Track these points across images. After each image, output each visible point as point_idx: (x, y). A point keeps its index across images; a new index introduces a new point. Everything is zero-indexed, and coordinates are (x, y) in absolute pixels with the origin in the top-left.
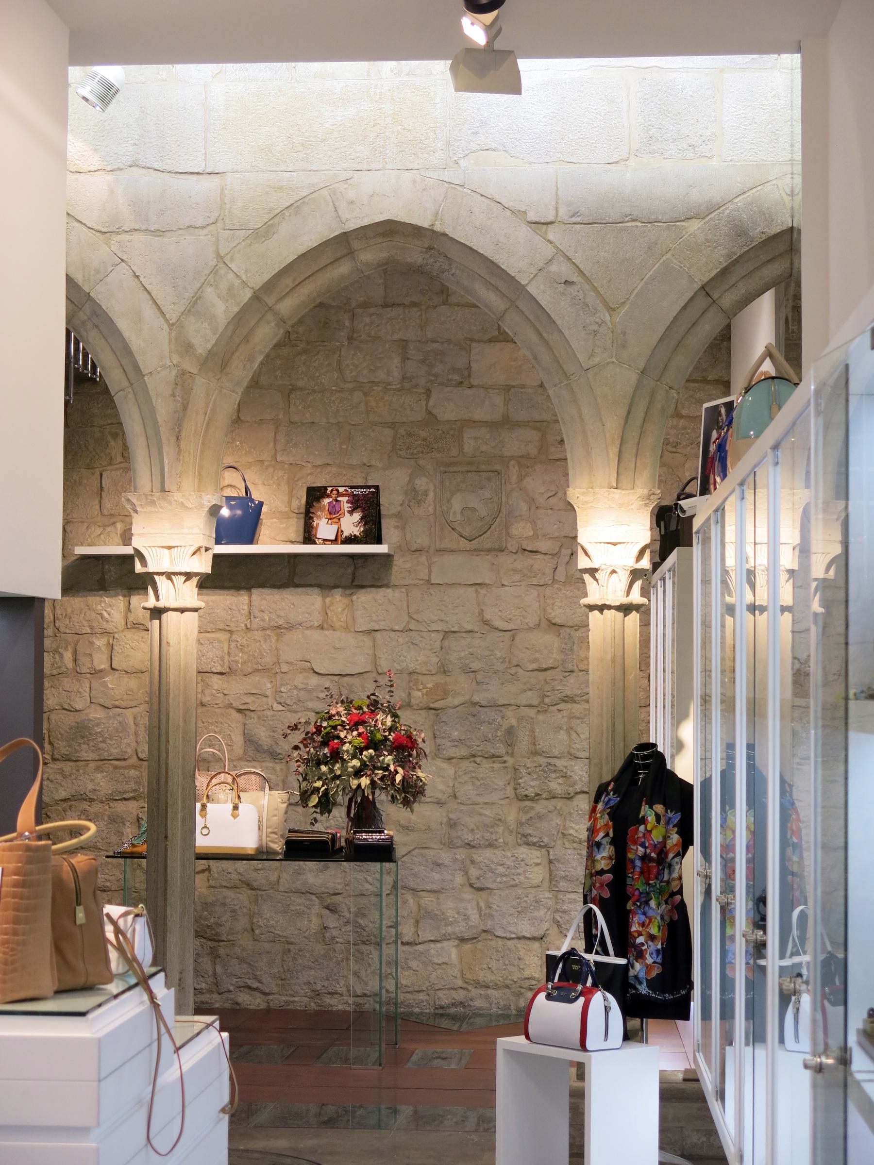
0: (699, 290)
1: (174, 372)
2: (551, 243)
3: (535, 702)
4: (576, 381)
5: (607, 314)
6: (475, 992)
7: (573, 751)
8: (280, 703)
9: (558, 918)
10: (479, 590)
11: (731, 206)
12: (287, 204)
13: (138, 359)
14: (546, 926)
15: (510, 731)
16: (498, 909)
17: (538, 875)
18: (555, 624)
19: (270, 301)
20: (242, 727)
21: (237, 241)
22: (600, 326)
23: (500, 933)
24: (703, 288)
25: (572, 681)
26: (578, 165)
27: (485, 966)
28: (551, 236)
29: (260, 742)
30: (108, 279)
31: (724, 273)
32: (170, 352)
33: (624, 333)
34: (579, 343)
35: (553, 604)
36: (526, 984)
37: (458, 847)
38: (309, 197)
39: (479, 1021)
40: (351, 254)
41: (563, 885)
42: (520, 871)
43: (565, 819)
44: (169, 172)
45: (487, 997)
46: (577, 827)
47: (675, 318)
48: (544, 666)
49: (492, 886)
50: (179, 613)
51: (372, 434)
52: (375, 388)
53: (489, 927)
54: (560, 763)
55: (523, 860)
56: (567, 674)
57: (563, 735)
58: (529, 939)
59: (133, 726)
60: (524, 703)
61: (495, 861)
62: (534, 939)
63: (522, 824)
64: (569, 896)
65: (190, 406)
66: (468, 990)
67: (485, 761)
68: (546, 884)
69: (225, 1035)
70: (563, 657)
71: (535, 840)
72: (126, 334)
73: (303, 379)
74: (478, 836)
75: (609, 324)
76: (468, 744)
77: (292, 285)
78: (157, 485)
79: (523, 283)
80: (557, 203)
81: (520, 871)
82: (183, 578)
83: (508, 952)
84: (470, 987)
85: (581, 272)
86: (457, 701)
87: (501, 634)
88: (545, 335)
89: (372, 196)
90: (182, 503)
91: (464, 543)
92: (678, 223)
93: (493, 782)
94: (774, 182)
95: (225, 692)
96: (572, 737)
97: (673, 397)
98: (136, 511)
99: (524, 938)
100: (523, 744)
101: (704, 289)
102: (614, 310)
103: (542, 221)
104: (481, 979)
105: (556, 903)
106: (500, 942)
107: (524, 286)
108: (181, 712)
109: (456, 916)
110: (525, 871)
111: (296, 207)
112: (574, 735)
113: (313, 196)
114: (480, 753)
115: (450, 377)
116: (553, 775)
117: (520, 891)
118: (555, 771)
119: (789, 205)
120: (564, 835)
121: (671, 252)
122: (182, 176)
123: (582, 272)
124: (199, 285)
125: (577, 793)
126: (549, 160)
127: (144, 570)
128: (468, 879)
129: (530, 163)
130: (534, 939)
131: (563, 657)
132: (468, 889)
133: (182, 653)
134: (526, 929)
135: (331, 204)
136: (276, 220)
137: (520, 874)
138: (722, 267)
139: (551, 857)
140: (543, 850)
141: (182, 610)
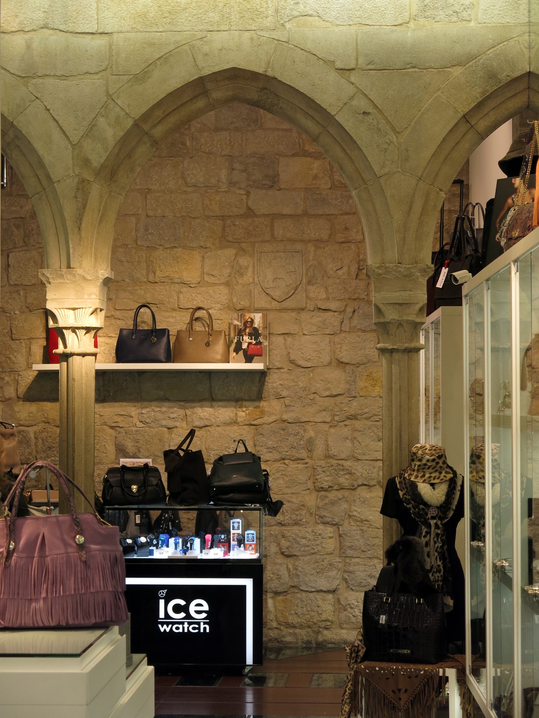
0: (462, 118)
1: (76, 180)
2: (353, 84)
3: (328, 419)
4: (372, 185)
5: (394, 137)
6: (285, 631)
7: (356, 455)
8: (142, 422)
9: (346, 577)
10: (286, 338)
11: (485, 57)
12: (158, 56)
13: (49, 170)
14: (337, 582)
15: (310, 442)
16: (302, 570)
17: (331, 545)
18: (342, 363)
19: (146, 128)
20: (114, 440)
21: (122, 84)
22: (389, 145)
23: (304, 588)
24: (464, 116)
25: (355, 404)
26: (372, 27)
27: (293, 612)
28: (353, 79)
29: (127, 450)
30: (27, 111)
31: (480, 105)
32: (73, 165)
33: (407, 151)
34: (373, 157)
35: (340, 348)
36: (323, 624)
37: (272, 526)
38: (175, 51)
39: (288, 652)
40: (205, 93)
41: (349, 552)
42: (318, 542)
43: (350, 505)
44: (71, 32)
45: (295, 634)
46: (359, 510)
47: (444, 139)
48: (335, 393)
49: (297, 554)
50: (81, 357)
51: (207, 225)
52: (209, 191)
53: (295, 584)
54: (347, 464)
55: (320, 535)
56: (351, 399)
57: (349, 444)
58: (325, 592)
59: (34, 440)
60: (319, 420)
61: (300, 535)
62: (329, 592)
63: (318, 508)
64: (354, 560)
65: (88, 205)
66: (280, 630)
67: (292, 462)
68: (337, 551)
69: (152, 668)
70: (348, 386)
71: (329, 520)
72: (41, 152)
73: (156, 184)
74: (287, 517)
75: (397, 145)
76: (280, 450)
77: (162, 116)
78: (64, 263)
79: (333, 113)
80: (357, 54)
81: (318, 542)
82: (84, 332)
83: (310, 601)
84: (282, 628)
85: (376, 107)
86: (271, 420)
87: (303, 370)
88: (348, 152)
89: (221, 50)
90: (84, 277)
91: (274, 304)
92: (446, 69)
93: (297, 478)
94: (516, 39)
95: (101, 414)
96: (355, 445)
97: (443, 196)
98: (49, 283)
99: (321, 591)
100: (319, 450)
101: (465, 118)
102: (399, 133)
103: (346, 68)
104: (290, 621)
105: (345, 566)
106: (304, 594)
107: (333, 116)
108: (83, 430)
109: (272, 576)
110: (321, 543)
111: (165, 59)
112: (356, 444)
113: (177, 50)
114: (288, 457)
115: (264, 182)
116: (342, 473)
117: (318, 557)
118: (343, 470)
119: (527, 56)
120: (350, 516)
121: (440, 91)
122: (80, 36)
123: (376, 106)
124: (94, 116)
125: (359, 486)
126: (351, 23)
127: (55, 326)
128: (280, 549)
129: (338, 25)
130: (329, 592)
131: (348, 386)
132: (280, 556)
133: (84, 386)
134: (322, 584)
135: (191, 56)
136: (150, 68)
137: (317, 545)
138: (478, 101)
139: (341, 532)
140: (335, 527)
141: (84, 355)
